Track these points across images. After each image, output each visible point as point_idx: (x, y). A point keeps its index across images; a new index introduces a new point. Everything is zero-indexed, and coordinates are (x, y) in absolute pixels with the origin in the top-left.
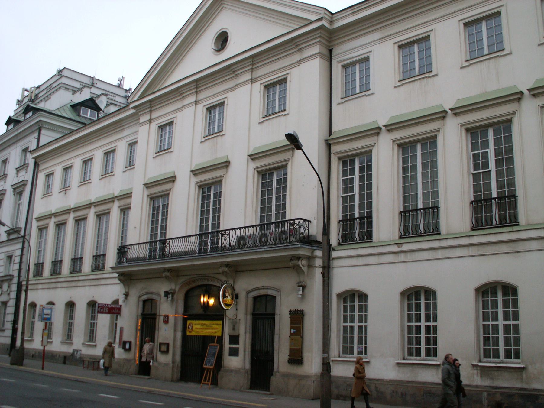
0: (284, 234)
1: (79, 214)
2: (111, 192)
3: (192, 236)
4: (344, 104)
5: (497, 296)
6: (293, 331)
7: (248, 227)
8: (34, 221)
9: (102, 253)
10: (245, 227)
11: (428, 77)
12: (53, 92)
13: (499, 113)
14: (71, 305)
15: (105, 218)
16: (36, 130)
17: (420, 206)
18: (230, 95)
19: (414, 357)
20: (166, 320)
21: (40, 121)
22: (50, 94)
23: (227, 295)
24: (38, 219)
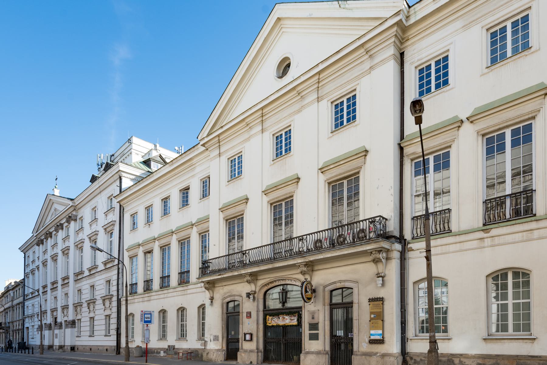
0: (363, 232)
2: (189, 221)
3: (223, 256)
7: (264, 246)
8: (125, 251)
9: (186, 270)
10: (262, 246)
13: (435, 144)
14: (182, 310)
15: (135, 259)
16: (117, 180)
18: (297, 117)
20: (249, 315)
23: (308, 290)
24: (128, 250)
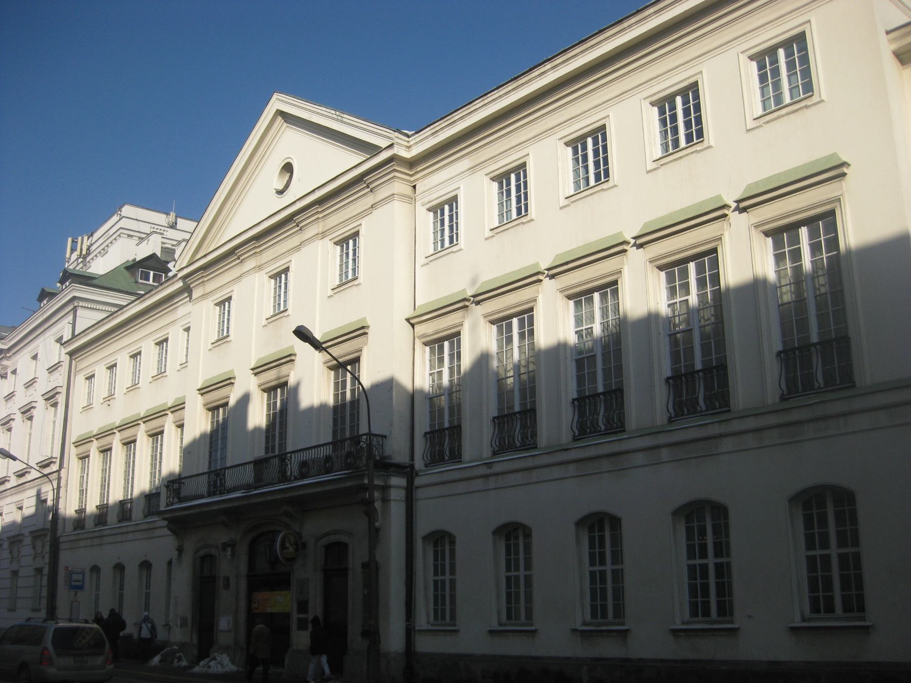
1: (128, 433)
4: (761, 129)
5: (826, 511)
11: (807, 107)
12: (111, 243)
17: (600, 389)
19: (822, 615)
21: (74, 298)
22: (107, 246)
23: (287, 545)
24: (77, 444)
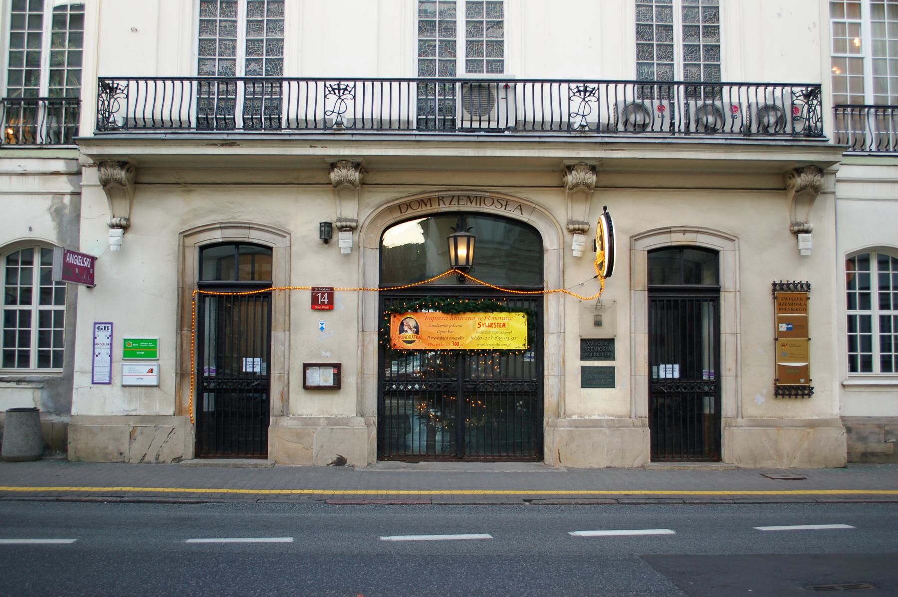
6: (783, 327)
